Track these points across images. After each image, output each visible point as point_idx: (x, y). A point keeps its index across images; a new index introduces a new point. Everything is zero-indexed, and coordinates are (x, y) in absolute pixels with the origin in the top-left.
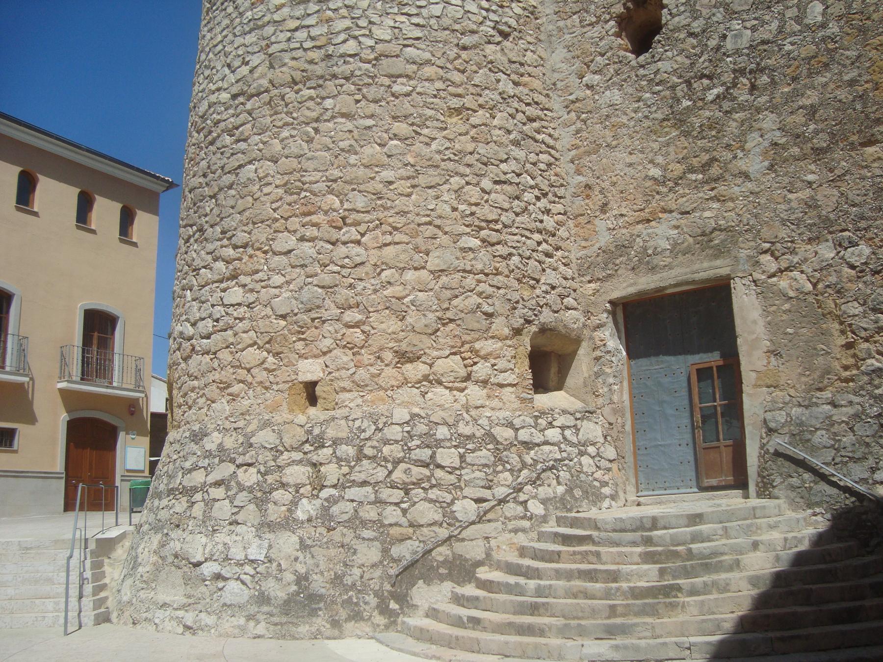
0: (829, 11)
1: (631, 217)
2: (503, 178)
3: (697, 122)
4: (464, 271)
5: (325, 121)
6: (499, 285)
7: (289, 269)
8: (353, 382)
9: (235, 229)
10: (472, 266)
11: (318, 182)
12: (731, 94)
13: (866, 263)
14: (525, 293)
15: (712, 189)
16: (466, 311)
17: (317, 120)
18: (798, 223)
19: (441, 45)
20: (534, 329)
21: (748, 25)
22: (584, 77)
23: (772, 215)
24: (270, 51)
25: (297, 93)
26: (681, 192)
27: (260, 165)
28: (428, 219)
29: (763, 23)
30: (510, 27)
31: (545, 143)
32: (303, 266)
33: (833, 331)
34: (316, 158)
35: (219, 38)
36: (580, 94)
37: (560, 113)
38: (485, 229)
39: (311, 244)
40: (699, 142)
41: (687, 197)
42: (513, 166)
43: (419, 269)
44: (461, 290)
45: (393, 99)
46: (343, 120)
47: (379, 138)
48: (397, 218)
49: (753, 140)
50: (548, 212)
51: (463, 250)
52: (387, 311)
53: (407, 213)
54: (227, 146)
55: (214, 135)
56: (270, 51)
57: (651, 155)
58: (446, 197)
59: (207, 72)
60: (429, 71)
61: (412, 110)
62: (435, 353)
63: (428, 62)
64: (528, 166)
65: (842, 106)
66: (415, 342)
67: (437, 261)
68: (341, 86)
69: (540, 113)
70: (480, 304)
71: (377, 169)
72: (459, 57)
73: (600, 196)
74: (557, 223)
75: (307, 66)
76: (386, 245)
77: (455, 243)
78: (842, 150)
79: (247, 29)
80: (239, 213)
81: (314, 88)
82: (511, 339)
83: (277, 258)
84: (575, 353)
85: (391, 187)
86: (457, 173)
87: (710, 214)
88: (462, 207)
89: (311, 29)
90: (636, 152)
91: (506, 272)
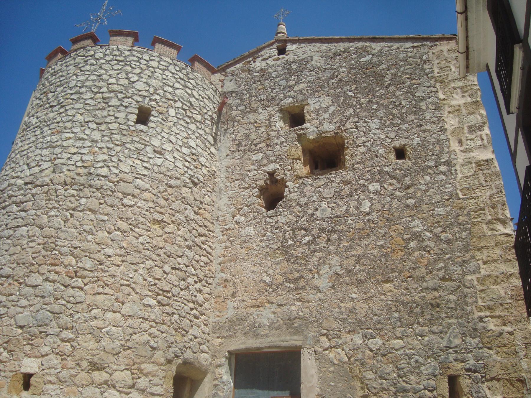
0: (373, 206)
1: (249, 302)
2: (177, 266)
3: (295, 254)
4: (143, 318)
5: (79, 211)
6: (163, 331)
7: (33, 297)
8: (58, 378)
9: (4, 265)
10: (149, 316)
11: (65, 246)
12: (316, 242)
13: (379, 349)
14: (178, 338)
15: (298, 294)
16: (140, 344)
17: (74, 209)
18: (344, 321)
19: (157, 182)
20: (180, 361)
21: (330, 205)
22: (235, 216)
23: (330, 314)
24: (56, 162)
25: (66, 190)
26: (280, 292)
27: (32, 228)
28: (128, 283)
29: (339, 206)
30: (199, 180)
31: (206, 251)
32: (43, 297)
33: (357, 387)
34: (68, 232)
35: (26, 147)
36: (231, 226)
37: (218, 235)
38: (161, 295)
39: (52, 284)
40: (294, 265)
41: (283, 297)
42: (184, 260)
43: (116, 312)
44: (139, 330)
45: (122, 207)
46: (89, 213)
47: (109, 228)
48: (109, 279)
49: (325, 269)
50: (200, 291)
51: (145, 305)
52: (90, 335)
53: (116, 276)
54: (13, 212)
55: (7, 203)
56: (56, 162)
57: (266, 268)
58: (141, 272)
59: (13, 165)
60: (147, 195)
61: (132, 216)
62: (115, 367)
63: (147, 190)
64: (194, 262)
65: (375, 259)
66: (103, 358)
67: (128, 309)
68: (93, 192)
69: (206, 232)
70: (149, 340)
71: (103, 247)
72: (166, 191)
73: (233, 287)
74: (205, 299)
75: (75, 176)
76: (98, 294)
77: (141, 300)
78: (372, 283)
79: (45, 146)
80: (10, 255)
81: (77, 190)
82: (164, 365)
83: (27, 289)
84: (202, 380)
85: (109, 259)
86: (150, 259)
87: (295, 308)
88: (149, 279)
89: (83, 155)
90: (257, 265)
91: (169, 324)
